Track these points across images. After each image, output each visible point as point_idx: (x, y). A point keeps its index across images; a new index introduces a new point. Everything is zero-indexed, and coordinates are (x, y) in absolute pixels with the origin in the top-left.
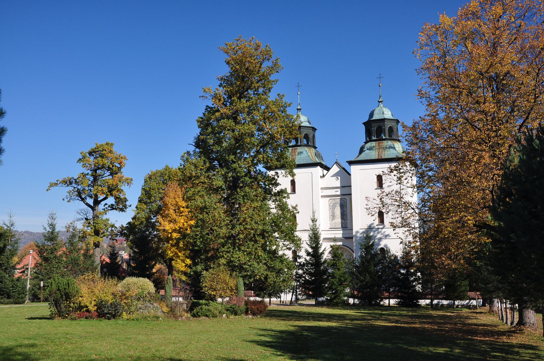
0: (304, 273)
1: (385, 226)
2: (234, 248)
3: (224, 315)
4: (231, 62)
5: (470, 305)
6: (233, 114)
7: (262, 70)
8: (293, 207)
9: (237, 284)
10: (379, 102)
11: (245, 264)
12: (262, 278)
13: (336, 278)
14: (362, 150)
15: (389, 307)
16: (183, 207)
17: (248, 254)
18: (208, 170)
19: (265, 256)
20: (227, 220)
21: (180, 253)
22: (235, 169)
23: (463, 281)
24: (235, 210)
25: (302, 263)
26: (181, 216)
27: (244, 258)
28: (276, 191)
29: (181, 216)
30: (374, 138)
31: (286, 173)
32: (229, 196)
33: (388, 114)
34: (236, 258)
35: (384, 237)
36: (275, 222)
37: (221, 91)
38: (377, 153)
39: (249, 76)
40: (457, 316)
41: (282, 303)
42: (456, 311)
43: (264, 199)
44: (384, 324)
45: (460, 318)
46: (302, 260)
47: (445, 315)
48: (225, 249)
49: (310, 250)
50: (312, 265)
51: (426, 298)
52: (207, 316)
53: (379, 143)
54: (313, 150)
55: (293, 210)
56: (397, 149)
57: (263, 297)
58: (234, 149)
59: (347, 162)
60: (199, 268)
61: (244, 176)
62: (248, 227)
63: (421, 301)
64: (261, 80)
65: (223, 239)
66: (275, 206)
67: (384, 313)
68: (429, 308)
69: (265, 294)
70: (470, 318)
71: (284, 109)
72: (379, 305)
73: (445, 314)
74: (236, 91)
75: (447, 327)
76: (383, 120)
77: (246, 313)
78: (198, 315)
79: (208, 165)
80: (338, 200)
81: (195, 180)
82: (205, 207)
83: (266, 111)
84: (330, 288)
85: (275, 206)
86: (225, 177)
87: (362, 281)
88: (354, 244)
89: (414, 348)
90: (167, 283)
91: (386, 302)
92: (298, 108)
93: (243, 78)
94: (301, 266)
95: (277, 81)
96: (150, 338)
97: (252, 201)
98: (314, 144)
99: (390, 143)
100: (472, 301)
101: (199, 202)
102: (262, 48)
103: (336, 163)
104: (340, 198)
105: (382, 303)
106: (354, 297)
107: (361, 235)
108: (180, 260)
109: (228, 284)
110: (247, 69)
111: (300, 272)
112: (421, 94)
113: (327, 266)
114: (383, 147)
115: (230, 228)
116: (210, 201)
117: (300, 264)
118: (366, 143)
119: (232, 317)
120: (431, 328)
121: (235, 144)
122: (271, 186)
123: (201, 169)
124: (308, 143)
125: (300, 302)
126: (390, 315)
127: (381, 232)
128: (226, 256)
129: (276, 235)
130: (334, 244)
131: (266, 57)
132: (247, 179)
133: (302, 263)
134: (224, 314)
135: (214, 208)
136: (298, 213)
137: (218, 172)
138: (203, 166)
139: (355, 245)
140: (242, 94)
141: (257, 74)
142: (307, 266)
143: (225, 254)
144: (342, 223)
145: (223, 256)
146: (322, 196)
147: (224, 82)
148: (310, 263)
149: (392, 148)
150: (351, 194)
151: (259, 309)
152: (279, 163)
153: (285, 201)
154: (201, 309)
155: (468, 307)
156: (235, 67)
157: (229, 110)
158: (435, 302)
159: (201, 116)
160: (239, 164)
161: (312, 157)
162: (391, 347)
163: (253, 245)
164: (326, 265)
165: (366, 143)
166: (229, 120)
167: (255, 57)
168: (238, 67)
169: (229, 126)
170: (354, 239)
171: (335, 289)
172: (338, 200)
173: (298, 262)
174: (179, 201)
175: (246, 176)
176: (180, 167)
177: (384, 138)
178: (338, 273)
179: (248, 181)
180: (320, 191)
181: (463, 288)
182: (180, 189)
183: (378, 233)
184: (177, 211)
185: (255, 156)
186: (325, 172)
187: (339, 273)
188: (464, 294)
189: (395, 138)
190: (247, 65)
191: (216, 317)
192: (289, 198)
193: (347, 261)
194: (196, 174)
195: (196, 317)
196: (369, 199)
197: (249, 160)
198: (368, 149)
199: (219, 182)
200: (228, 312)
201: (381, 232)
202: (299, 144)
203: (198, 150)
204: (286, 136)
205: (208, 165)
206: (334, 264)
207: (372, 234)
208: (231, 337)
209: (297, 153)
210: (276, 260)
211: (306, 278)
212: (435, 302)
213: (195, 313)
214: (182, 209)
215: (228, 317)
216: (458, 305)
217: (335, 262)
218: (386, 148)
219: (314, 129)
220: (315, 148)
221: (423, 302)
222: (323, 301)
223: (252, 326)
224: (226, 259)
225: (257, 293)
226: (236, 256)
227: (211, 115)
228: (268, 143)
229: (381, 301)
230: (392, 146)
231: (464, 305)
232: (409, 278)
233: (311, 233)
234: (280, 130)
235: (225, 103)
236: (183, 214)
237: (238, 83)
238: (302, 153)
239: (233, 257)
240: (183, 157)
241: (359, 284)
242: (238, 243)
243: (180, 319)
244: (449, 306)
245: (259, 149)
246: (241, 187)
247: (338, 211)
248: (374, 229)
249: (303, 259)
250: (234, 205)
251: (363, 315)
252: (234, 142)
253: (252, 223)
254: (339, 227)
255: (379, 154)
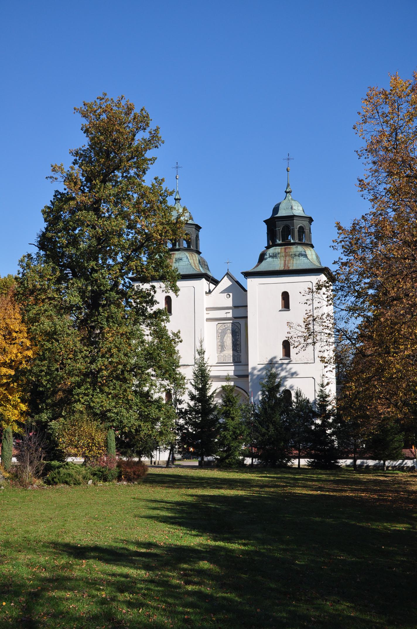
0: (186, 424)
1: (291, 361)
2: (94, 389)
3: (90, 482)
4: (90, 129)
5: (403, 467)
6: (95, 203)
7: (135, 143)
8: (173, 334)
9: (107, 439)
10: (286, 192)
11: (109, 411)
12: (133, 431)
13: (229, 430)
14: (262, 258)
15: (299, 470)
16: (17, 332)
17: (113, 398)
18: (59, 281)
19: (137, 401)
20: (86, 350)
21: (11, 395)
22: (96, 280)
23: (396, 434)
24: (95, 337)
25: (183, 410)
26: (14, 344)
27: (108, 404)
28: (152, 312)
29: (14, 344)
30: (278, 242)
31: (166, 287)
32: (88, 316)
33: (298, 210)
34: (98, 403)
35: (289, 376)
36: (151, 354)
37: (77, 172)
38: (283, 262)
39: (118, 151)
40: (393, 481)
41: (153, 464)
42: (390, 475)
43: (136, 322)
44: (307, 492)
45: (399, 483)
46: (184, 406)
47: (376, 480)
48: (82, 390)
49: (196, 393)
50: (197, 412)
51: (347, 458)
52: (66, 483)
53: (285, 249)
54: (196, 257)
55: (174, 338)
56: (309, 257)
57: (131, 456)
58: (96, 253)
59: (242, 273)
60: (44, 416)
61: (110, 291)
62: (114, 360)
63: (341, 461)
64: (132, 158)
65: (78, 376)
66: (149, 331)
67: (297, 477)
68: (352, 470)
69: (133, 451)
70: (411, 484)
71: (164, 199)
72: (285, 466)
73: (377, 478)
74: (99, 172)
75: (390, 496)
76: (292, 218)
77: (119, 479)
78: (55, 482)
79: (58, 274)
80: (229, 325)
81: (40, 294)
82: (55, 333)
83: (141, 200)
84: (221, 444)
85: (149, 331)
86: (82, 292)
87: (263, 435)
88: (250, 384)
89: (364, 524)
90: (5, 437)
91: (296, 462)
92: (177, 198)
93: (108, 153)
94: (182, 414)
95: (154, 159)
96: (6, 515)
97: (120, 325)
98: (197, 248)
99: (300, 249)
100: (406, 461)
101: (46, 325)
102: (137, 110)
103: (227, 274)
104: (231, 322)
105: (289, 464)
106: (252, 455)
107: (259, 373)
108: (11, 405)
109: (93, 439)
110: (114, 141)
111: (182, 421)
112: (362, 184)
113: (218, 414)
114: (291, 253)
115: (89, 361)
116: (61, 323)
117: (181, 412)
118: (268, 248)
119: (101, 484)
120: (369, 497)
121: (97, 245)
122: (144, 305)
123: (49, 280)
124: (189, 246)
125: (177, 463)
126: (307, 480)
127: (286, 368)
128: (83, 401)
129: (150, 371)
130: (227, 384)
131: (141, 126)
132: (113, 294)
133: (183, 410)
134: (90, 480)
135: (67, 334)
136: (181, 342)
137: (73, 284)
138: (51, 275)
139: (252, 386)
140: (106, 175)
141: (128, 148)
142: (190, 414)
143: (82, 398)
144: (234, 356)
145: (79, 401)
146: (208, 320)
147: (80, 158)
148: (195, 410)
149: (302, 255)
150: (246, 317)
151: (137, 473)
152: (158, 273)
153: (163, 325)
154: (59, 473)
155: (401, 468)
156: (98, 138)
157: (89, 198)
158: (359, 462)
159: (49, 205)
160: (102, 274)
161: (195, 266)
162: (334, 522)
163: (121, 386)
164: (215, 413)
165: (268, 248)
166: (88, 212)
167: (126, 125)
168: (101, 137)
169: (89, 221)
170: (250, 378)
171: (228, 445)
172: (228, 325)
173: (178, 409)
174: (10, 323)
175: (111, 290)
176: (17, 276)
177: (292, 241)
178: (231, 424)
179: (115, 297)
180: (205, 312)
181: (397, 444)
182: (12, 307)
183: (282, 370)
184: (8, 337)
185: (123, 264)
186: (212, 286)
187: (233, 423)
188: (397, 452)
189: (306, 242)
190: (115, 135)
191: (79, 484)
192: (169, 321)
193: (243, 407)
194: (42, 285)
195: (52, 485)
196: (291, 325)
197: (117, 268)
198: (270, 257)
199: (76, 299)
200: (95, 477)
201: (286, 368)
202: (177, 247)
203: (42, 253)
204: (168, 236)
205: (58, 274)
206: (227, 411)
207: (274, 370)
208: (117, 512)
209: (174, 260)
210: (151, 406)
211: (188, 431)
212: (359, 462)
213: (50, 479)
214: (14, 334)
215: (95, 484)
216: (388, 467)
217: (228, 408)
218: (295, 255)
219: (198, 228)
220: (199, 253)
221: (344, 462)
222: (209, 462)
223: (136, 496)
224: (83, 404)
225: (122, 450)
226: (98, 400)
227: (64, 204)
228: (142, 245)
229: (288, 461)
230: (303, 253)
231: (395, 466)
232: (326, 430)
233: (197, 369)
234: (160, 227)
235: (82, 188)
236: (17, 341)
237: (102, 160)
238: (181, 259)
239: (94, 402)
240: (21, 261)
241: (260, 439)
242: (100, 382)
243: (30, 488)
244: (376, 468)
245: (131, 254)
246: (104, 306)
247: (228, 340)
248: (276, 365)
249: (186, 405)
250: (94, 330)
251: (272, 481)
252: (95, 243)
253: (120, 354)
254: (229, 361)
255: (285, 264)
